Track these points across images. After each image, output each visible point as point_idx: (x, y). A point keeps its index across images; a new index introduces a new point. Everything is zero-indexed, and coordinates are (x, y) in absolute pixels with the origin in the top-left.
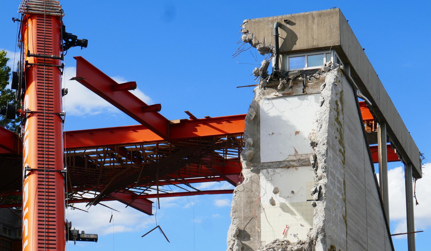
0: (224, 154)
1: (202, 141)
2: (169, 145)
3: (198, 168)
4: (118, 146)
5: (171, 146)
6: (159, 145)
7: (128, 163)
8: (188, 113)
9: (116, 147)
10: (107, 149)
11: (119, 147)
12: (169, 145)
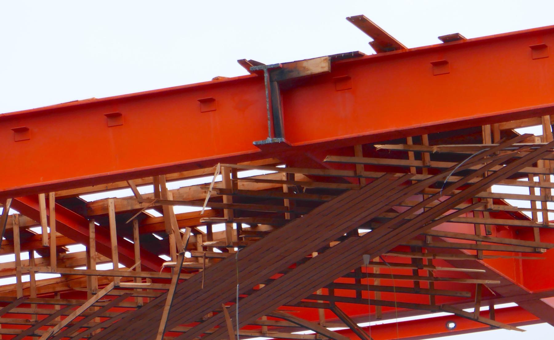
0: (532, 198)
1: (435, 149)
2: (283, 176)
3: (416, 273)
4: (52, 195)
5: (291, 177)
6: (240, 175)
7: (100, 267)
8: (361, 22)
9: (42, 197)
10: (239, 226)
11: (223, 216)
12: (283, 176)
